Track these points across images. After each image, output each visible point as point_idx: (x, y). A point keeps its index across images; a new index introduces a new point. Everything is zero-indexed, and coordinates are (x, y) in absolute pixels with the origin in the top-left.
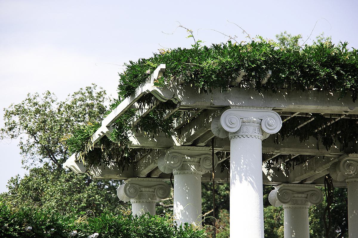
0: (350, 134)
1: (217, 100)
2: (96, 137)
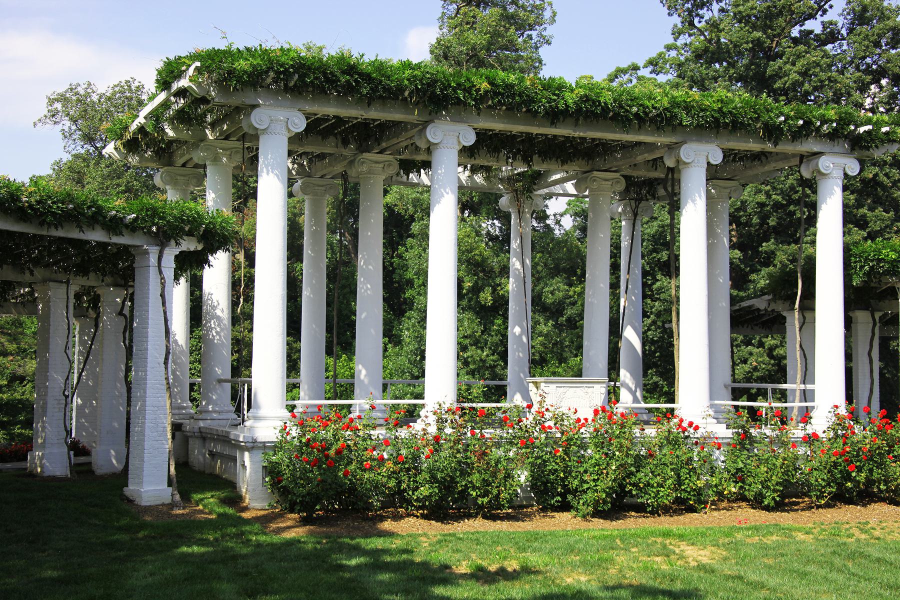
1: (248, 98)
2: (134, 127)
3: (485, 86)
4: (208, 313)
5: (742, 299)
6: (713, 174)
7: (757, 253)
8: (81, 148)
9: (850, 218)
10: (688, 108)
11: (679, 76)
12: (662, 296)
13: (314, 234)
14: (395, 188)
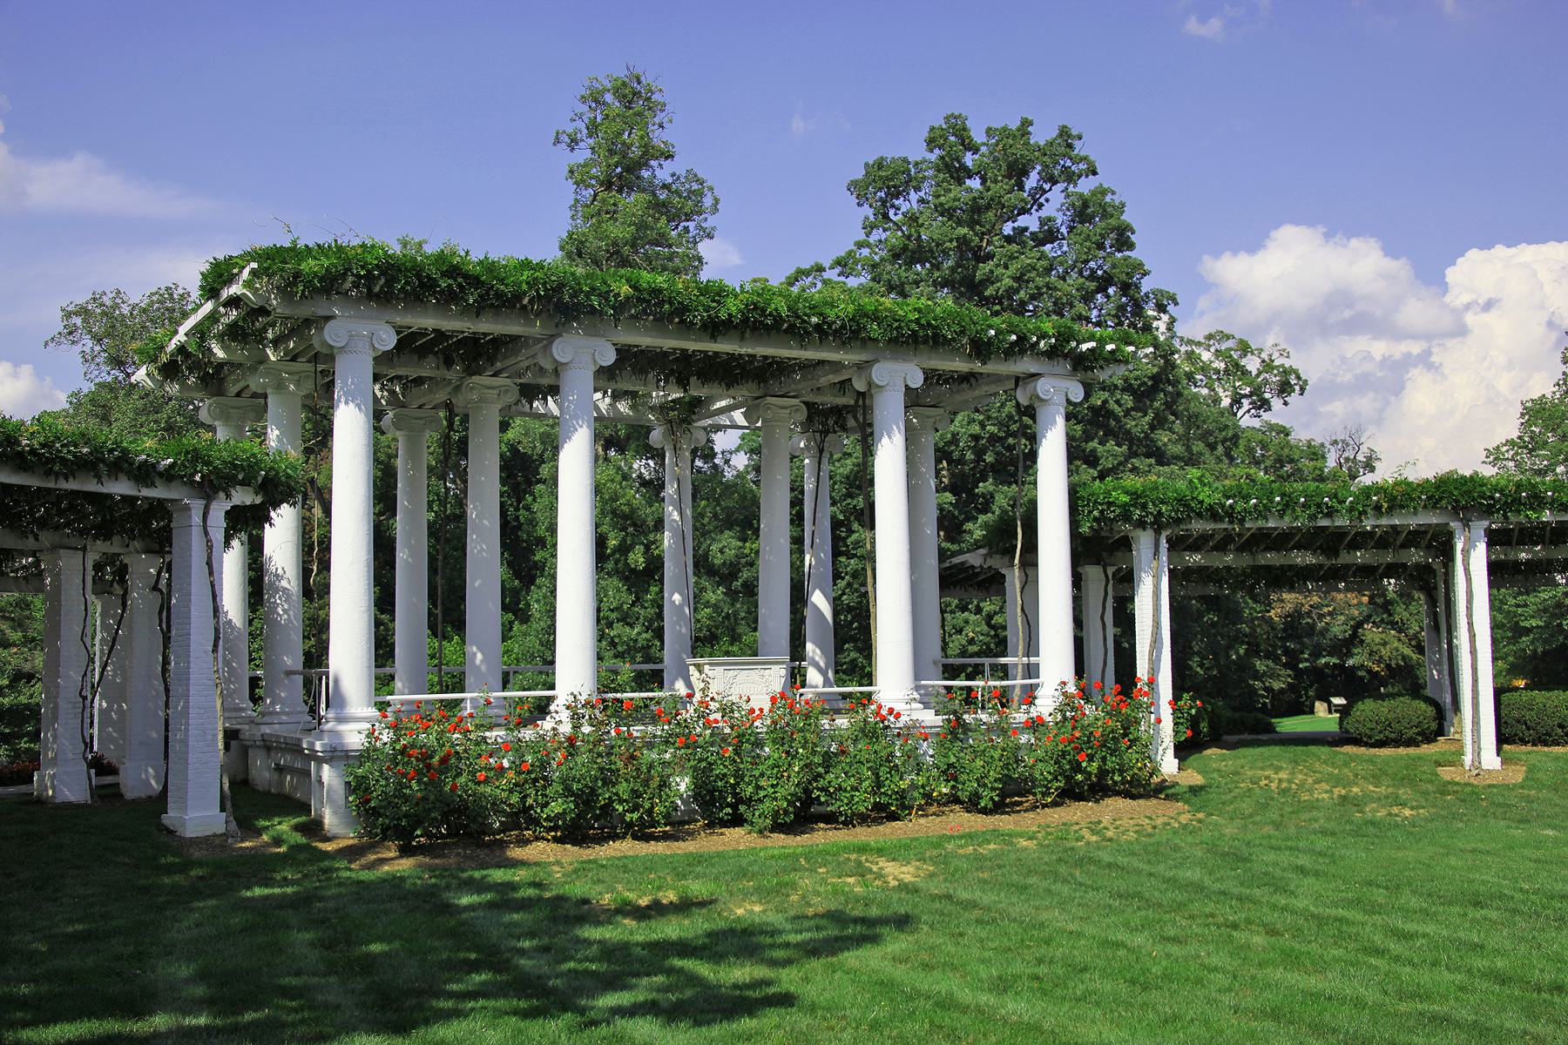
1: (319, 308)
2: (172, 346)
3: (625, 290)
4: (271, 584)
5: (954, 554)
6: (913, 399)
7: (973, 497)
8: (108, 375)
9: (1076, 454)
10: (875, 316)
11: (873, 279)
12: (859, 552)
13: (411, 481)
14: (518, 421)
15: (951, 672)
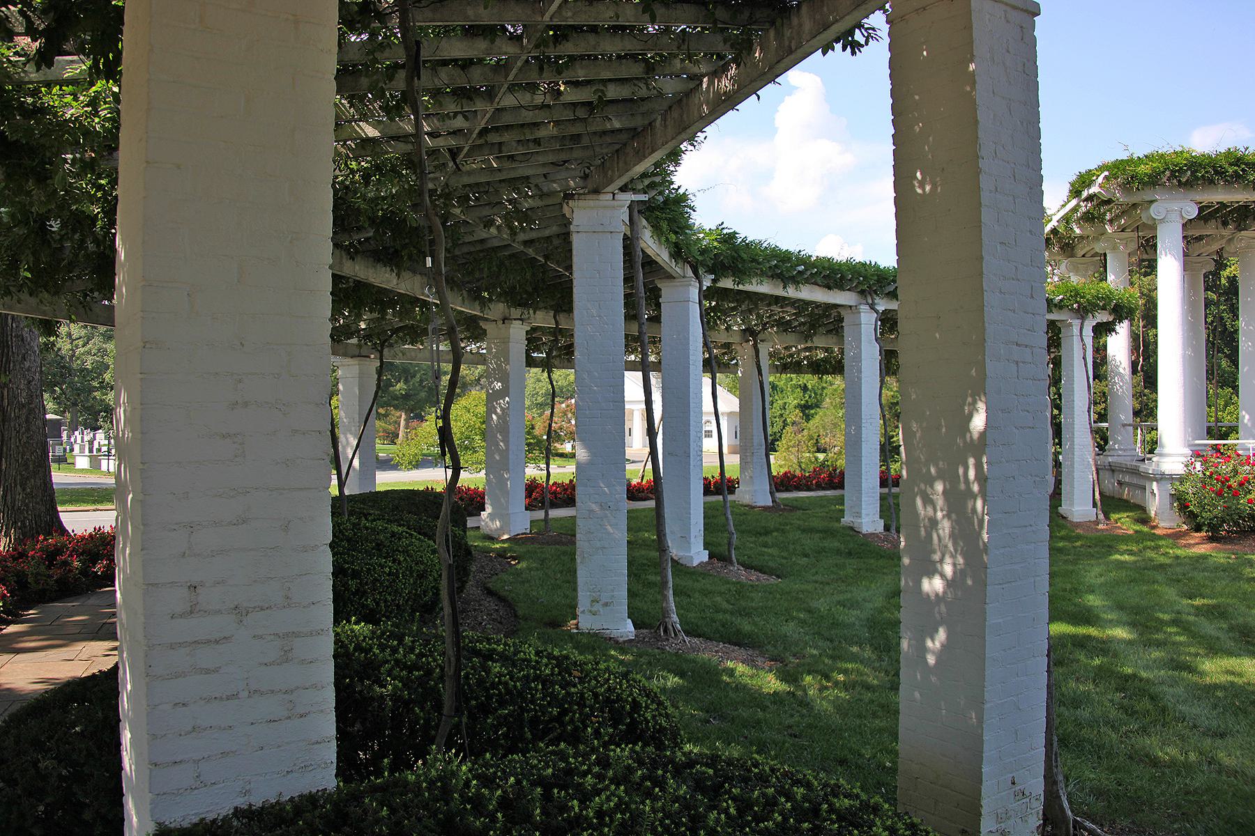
0: (1243, 216)
1: (1147, 195)
15: (1210, 433)
